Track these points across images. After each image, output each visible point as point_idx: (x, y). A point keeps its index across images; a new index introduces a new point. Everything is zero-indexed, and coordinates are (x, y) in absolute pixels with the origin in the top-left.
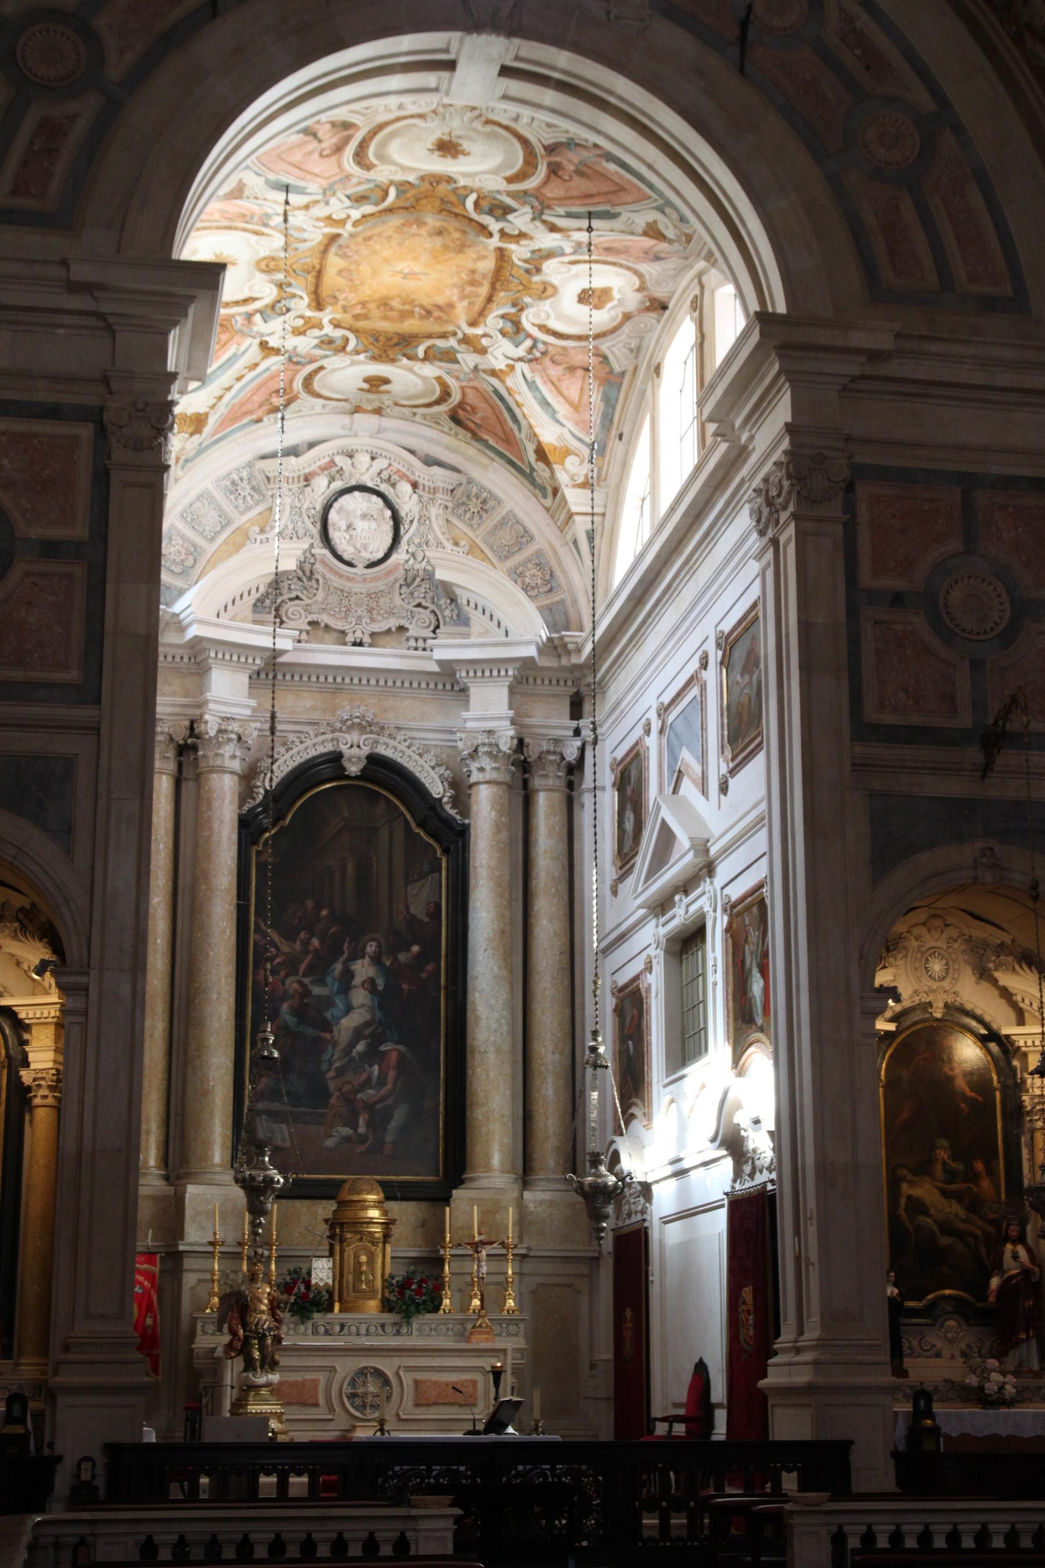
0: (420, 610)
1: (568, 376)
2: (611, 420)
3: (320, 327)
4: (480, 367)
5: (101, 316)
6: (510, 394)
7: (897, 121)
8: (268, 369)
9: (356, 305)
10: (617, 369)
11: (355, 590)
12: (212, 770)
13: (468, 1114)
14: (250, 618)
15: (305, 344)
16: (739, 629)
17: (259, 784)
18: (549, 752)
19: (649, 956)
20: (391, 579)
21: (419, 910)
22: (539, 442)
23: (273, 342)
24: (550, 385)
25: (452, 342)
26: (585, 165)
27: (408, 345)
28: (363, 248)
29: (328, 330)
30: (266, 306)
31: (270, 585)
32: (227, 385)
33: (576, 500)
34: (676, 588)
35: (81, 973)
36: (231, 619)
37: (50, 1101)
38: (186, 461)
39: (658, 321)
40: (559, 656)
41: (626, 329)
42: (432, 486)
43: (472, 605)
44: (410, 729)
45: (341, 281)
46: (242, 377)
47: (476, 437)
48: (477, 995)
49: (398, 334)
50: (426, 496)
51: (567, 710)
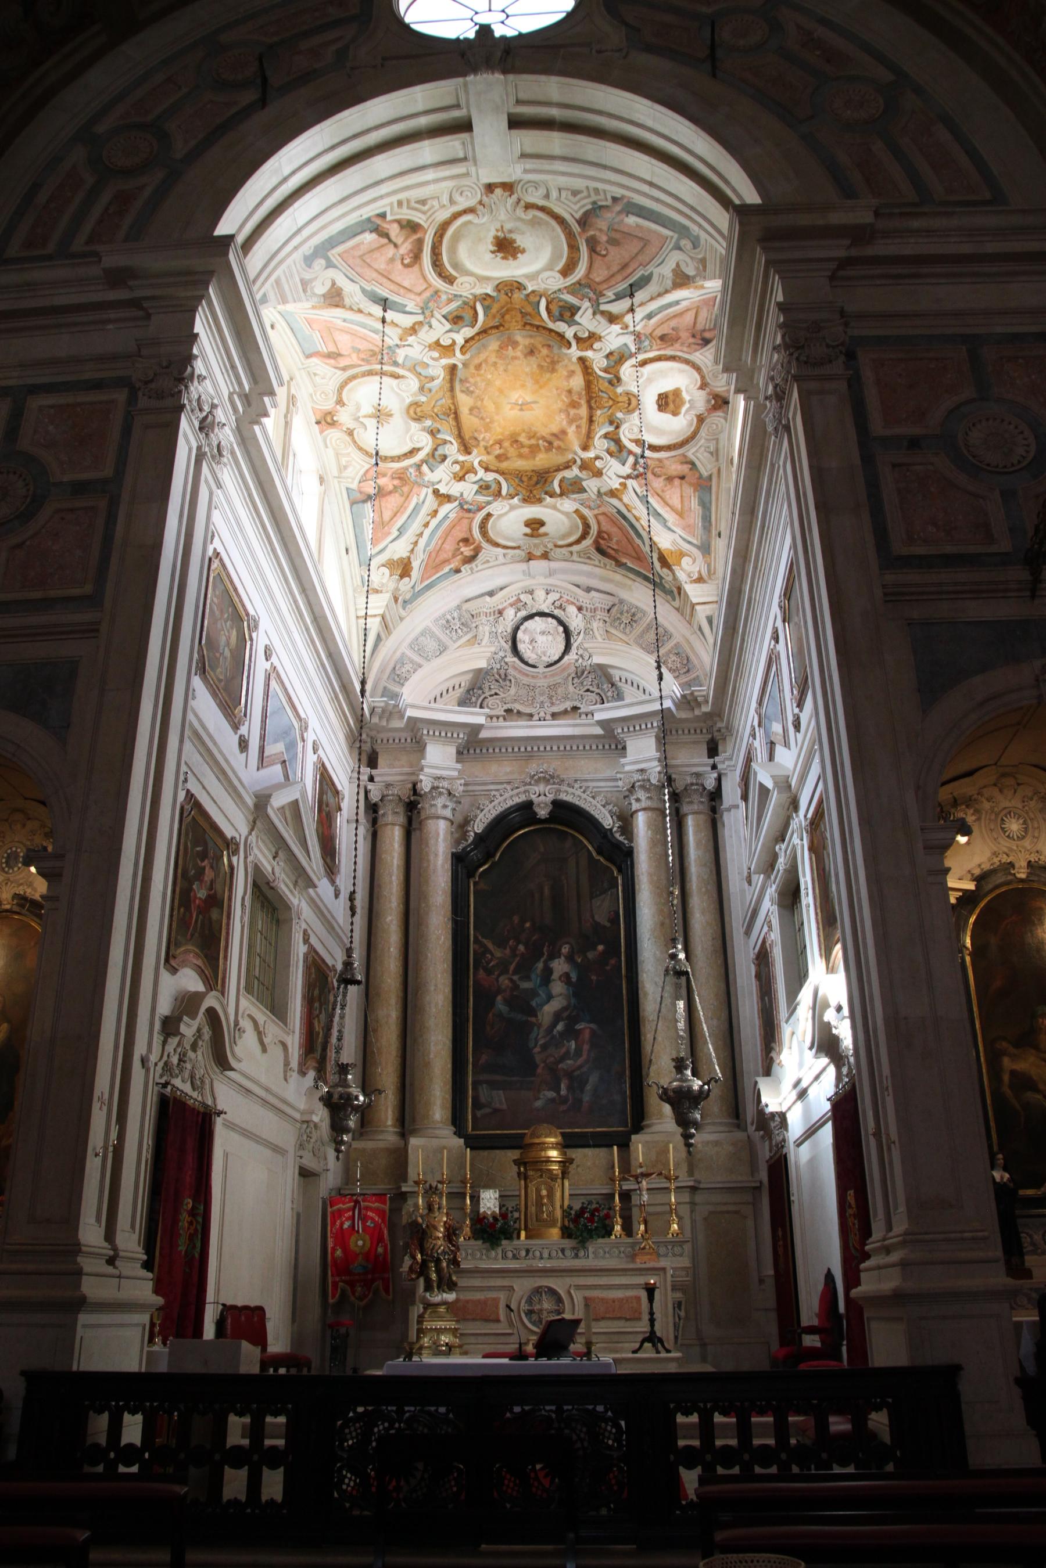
1: (669, 487)
2: (710, 521)
4: (602, 491)
6: (629, 511)
10: (705, 474)
15: (467, 489)
18: (692, 784)
20: (566, 674)
21: (602, 918)
23: (443, 490)
24: (656, 497)
25: (575, 472)
29: (481, 473)
32: (418, 532)
33: (695, 593)
40: (693, 709)
43: (623, 680)
44: (586, 781)
46: (428, 523)
47: (619, 564)
50: (589, 614)
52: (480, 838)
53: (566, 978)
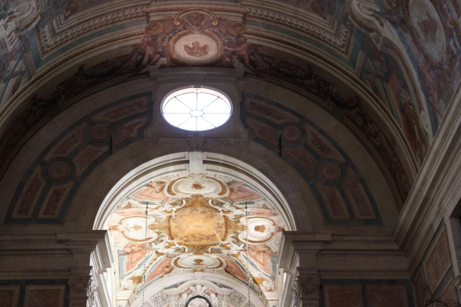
1: (258, 255)
2: (276, 268)
3: (175, 245)
5: (68, 250)
6: (240, 262)
7: (333, 166)
8: (160, 260)
15: (171, 251)
23: (160, 251)
24: (253, 258)
25: (218, 247)
26: (240, 188)
27: (205, 248)
28: (180, 219)
29: (177, 246)
30: (155, 240)
33: (268, 296)
38: (138, 292)
41: (274, 238)
42: (222, 294)
45: (177, 230)
46: (152, 263)
47: (235, 277)
50: (220, 297)
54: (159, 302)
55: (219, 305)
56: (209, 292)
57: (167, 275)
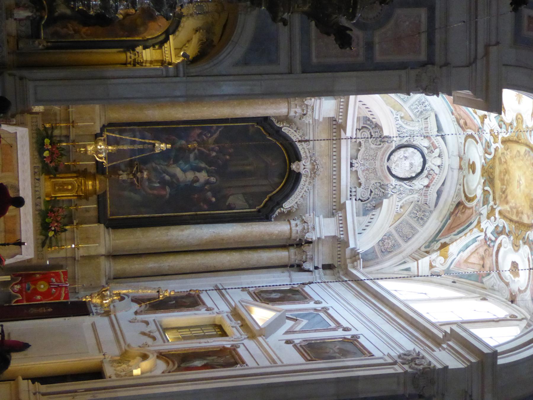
0: (369, 193)
2: (461, 278)
3: (495, 142)
4: (481, 216)
5: (476, 58)
6: (470, 230)
8: (475, 118)
9: (505, 159)
10: (484, 280)
11: (376, 162)
12: (289, 103)
13: (139, 229)
14: (360, 116)
16: (359, 346)
17: (284, 124)
18: (307, 255)
19: (213, 309)
20: (383, 178)
21: (231, 200)
22: (449, 244)
24: (475, 249)
25: (492, 203)
31: (376, 123)
33: (424, 262)
34: (381, 314)
35: (184, 73)
36: (359, 107)
37: (129, 60)
39: (506, 299)
40: (351, 258)
41: (502, 284)
42: (428, 194)
43: (372, 217)
45: (515, 152)
47: (452, 214)
48: (193, 230)
49: (494, 178)
51: (327, 263)
52: (278, 131)
53: (196, 180)
54: (418, 107)
55: (413, 190)
56: (430, 176)
57: (455, 119)
